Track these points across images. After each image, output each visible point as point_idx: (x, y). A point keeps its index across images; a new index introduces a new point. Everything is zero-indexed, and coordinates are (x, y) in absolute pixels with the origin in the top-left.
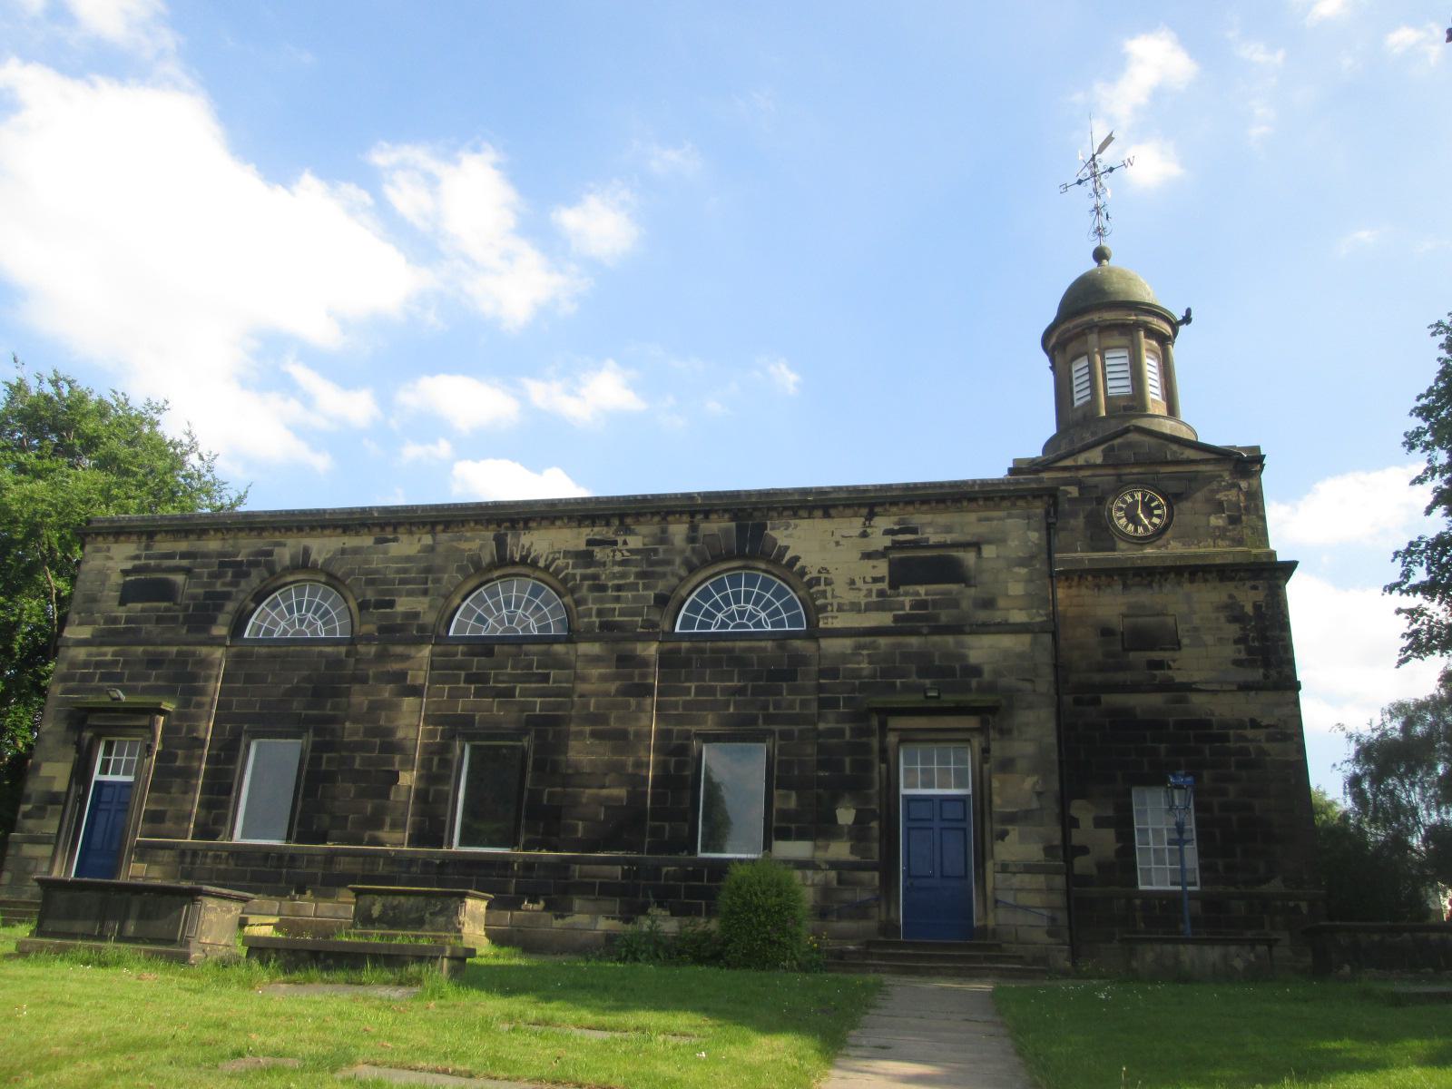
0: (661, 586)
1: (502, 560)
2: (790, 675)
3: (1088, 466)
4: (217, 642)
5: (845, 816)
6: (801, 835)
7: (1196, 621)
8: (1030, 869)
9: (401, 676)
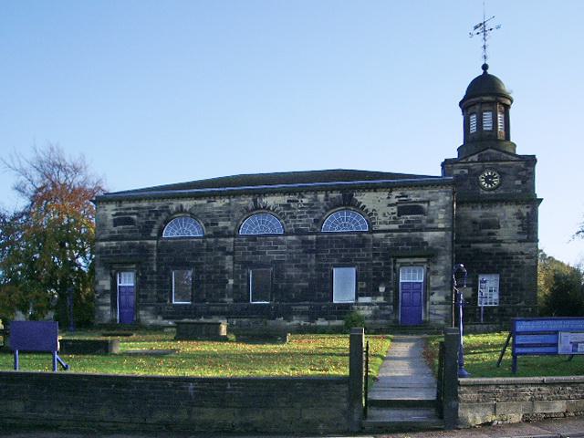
0: (316, 216)
5: (382, 289)
7: (506, 219)
8: (440, 303)
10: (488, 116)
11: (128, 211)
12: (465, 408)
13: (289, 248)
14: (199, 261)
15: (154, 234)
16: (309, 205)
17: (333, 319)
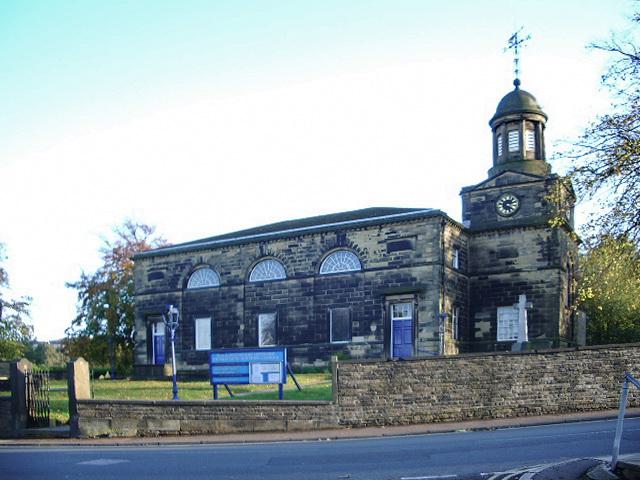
0: (314, 259)
1: (263, 255)
3: (491, 187)
4: (179, 290)
5: (373, 328)
6: (361, 335)
7: (525, 246)
8: (429, 340)
9: (236, 296)
10: (513, 136)
11: (160, 266)
12: (83, 421)
13: (290, 292)
14: (216, 308)
15: (180, 286)
16: (308, 248)
17: (201, 364)
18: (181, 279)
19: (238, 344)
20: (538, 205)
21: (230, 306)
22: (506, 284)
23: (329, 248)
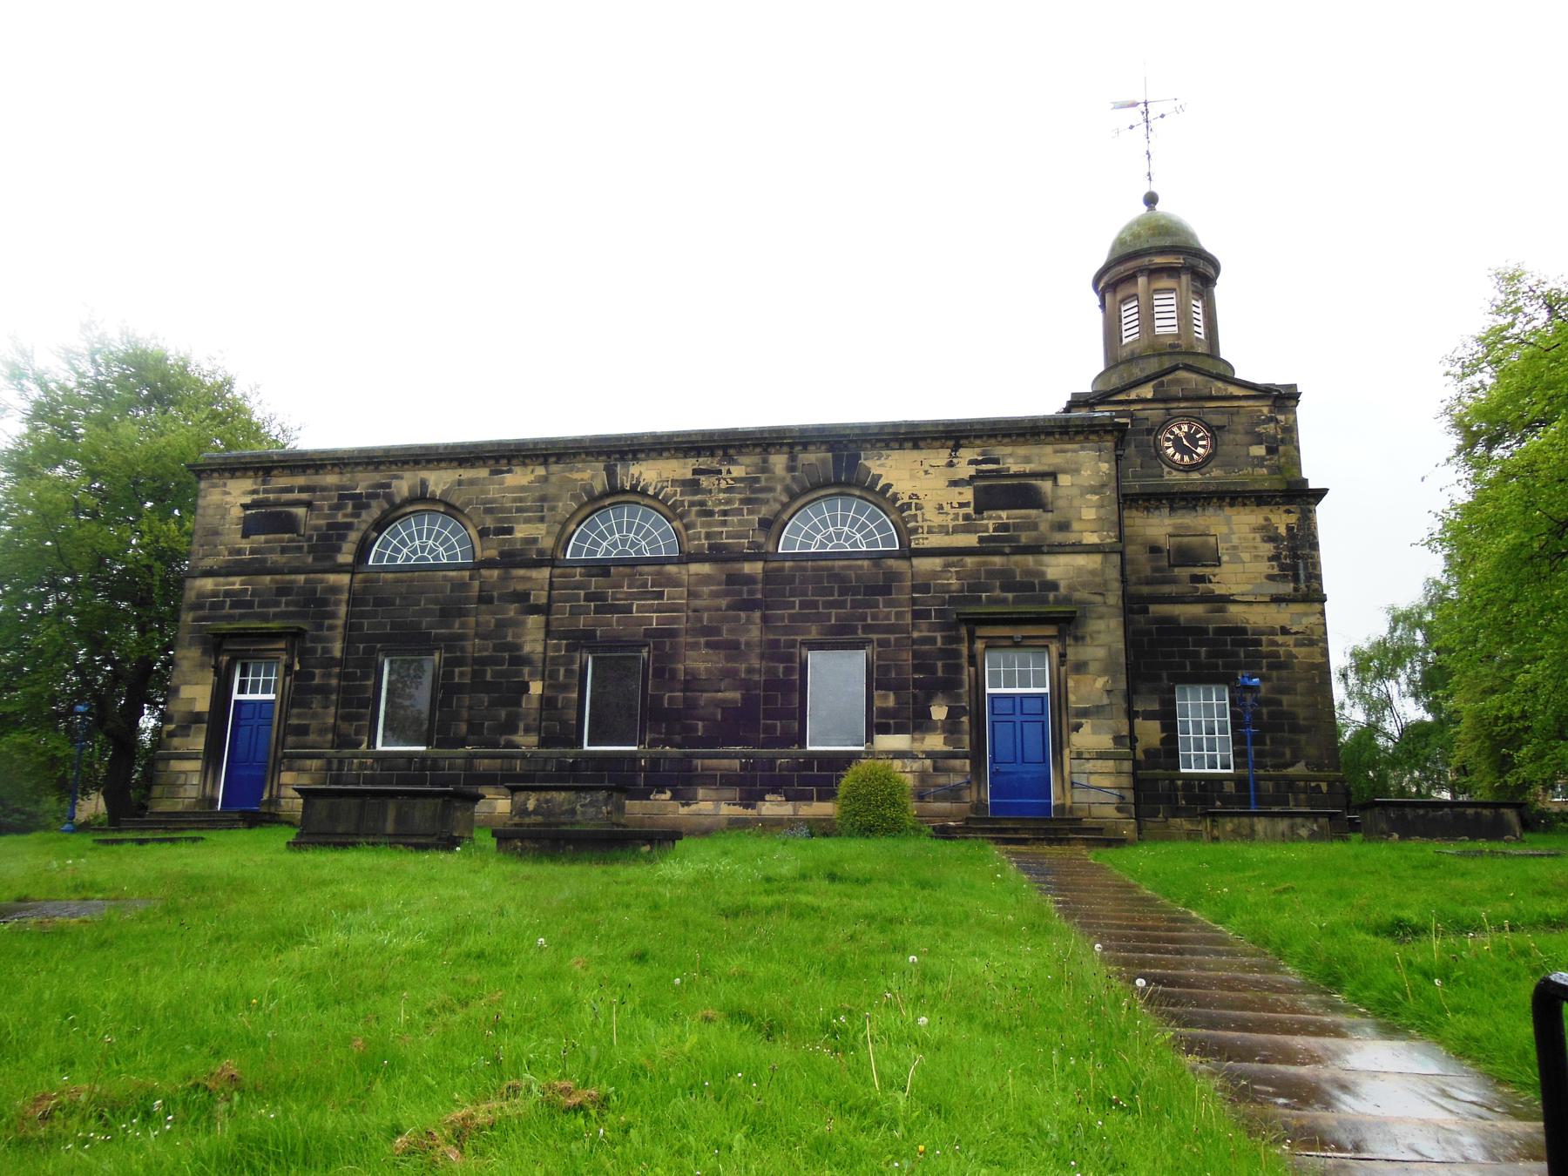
0: (764, 511)
2: (885, 590)
4: (340, 569)
5: (939, 712)
6: (900, 730)
7: (1235, 541)
8: (1102, 756)
13: (692, 594)
14: (456, 629)
15: (345, 558)
16: (750, 481)
18: (354, 536)
19: (518, 738)
20: (1259, 451)
21: (501, 625)
22: (1196, 631)
23: (806, 490)
